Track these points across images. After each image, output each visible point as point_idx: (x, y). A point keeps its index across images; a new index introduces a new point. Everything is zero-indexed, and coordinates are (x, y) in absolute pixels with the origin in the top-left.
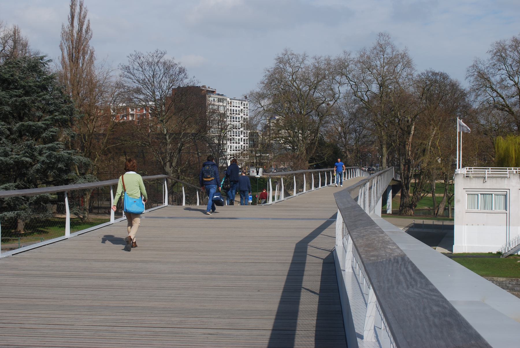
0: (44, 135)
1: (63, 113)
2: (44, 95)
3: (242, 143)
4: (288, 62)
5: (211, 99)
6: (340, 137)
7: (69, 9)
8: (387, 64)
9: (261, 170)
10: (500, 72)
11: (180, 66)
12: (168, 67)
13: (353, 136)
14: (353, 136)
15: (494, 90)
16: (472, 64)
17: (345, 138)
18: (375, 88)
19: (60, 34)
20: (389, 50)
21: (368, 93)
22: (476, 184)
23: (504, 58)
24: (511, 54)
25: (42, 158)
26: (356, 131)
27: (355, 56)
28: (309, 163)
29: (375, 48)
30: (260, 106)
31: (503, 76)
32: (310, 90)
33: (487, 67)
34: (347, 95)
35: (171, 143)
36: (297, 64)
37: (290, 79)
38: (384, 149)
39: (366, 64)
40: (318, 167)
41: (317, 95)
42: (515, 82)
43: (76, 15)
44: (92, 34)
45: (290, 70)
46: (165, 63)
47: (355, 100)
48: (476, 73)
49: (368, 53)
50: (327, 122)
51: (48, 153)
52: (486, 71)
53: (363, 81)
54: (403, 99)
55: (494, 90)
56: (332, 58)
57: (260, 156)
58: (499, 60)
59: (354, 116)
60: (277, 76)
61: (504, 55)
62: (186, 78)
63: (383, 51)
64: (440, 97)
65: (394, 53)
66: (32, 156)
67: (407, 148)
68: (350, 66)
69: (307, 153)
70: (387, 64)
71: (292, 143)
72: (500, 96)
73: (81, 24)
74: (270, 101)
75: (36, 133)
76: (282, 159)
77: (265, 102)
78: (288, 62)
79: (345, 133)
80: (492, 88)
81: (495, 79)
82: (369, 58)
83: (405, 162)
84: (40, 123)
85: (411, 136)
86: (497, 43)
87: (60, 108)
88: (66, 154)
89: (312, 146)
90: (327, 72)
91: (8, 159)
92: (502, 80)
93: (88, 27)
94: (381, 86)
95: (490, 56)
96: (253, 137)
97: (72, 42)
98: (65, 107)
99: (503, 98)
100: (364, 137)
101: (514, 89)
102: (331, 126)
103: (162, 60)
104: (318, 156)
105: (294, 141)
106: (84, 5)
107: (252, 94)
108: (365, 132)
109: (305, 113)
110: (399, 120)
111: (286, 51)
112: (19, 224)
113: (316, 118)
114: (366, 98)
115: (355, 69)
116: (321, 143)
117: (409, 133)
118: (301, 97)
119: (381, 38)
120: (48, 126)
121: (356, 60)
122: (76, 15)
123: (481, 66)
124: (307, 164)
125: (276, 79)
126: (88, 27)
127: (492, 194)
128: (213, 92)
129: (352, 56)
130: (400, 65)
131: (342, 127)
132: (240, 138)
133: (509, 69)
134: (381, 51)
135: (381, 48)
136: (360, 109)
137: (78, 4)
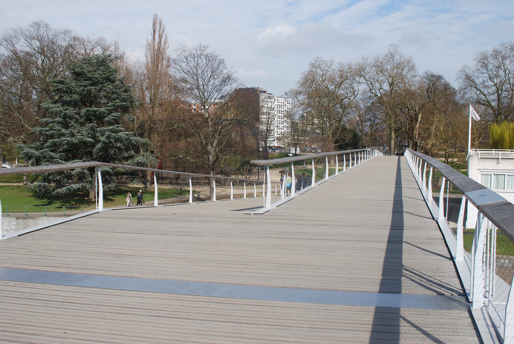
0: (106, 119)
1: (123, 100)
2: (108, 85)
3: (285, 129)
4: (319, 66)
5: (262, 96)
6: (358, 125)
7: (152, 26)
8: (396, 68)
9: (298, 149)
10: (483, 75)
11: (219, 57)
12: (209, 58)
13: (368, 124)
14: (368, 124)
15: (477, 89)
16: (461, 69)
17: (362, 125)
18: (386, 87)
19: (145, 45)
20: (397, 57)
21: (381, 91)
22: (490, 165)
23: (486, 65)
24: (492, 61)
25: (102, 139)
26: (370, 120)
27: (371, 61)
28: (335, 144)
29: (387, 56)
30: (297, 100)
31: (485, 79)
32: (336, 88)
33: (472, 72)
34: (365, 92)
35: (212, 126)
36: (326, 68)
37: (321, 79)
38: (393, 134)
39: (380, 68)
40: (341, 148)
41: (341, 92)
42: (494, 83)
43: (157, 28)
44: (169, 45)
45: (320, 72)
46: (207, 56)
47: (370, 96)
48: (464, 76)
49: (381, 59)
50: (348, 113)
51: (107, 133)
52: (472, 74)
53: (377, 80)
54: (409, 94)
55: (477, 89)
56: (353, 64)
57: (298, 139)
58: (482, 66)
59: (369, 109)
60: (310, 77)
61: (486, 62)
62: (226, 68)
63: (393, 58)
64: (437, 95)
65: (402, 59)
66: (94, 137)
67: (415, 133)
68: (367, 69)
69: (333, 136)
70: (396, 68)
71: (322, 129)
72: (483, 94)
73: (160, 37)
74: (305, 97)
75: (100, 119)
76: (314, 140)
77: (301, 97)
78: (319, 66)
79: (362, 122)
80: (476, 87)
81: (478, 81)
82: (382, 63)
83: (413, 144)
84: (103, 109)
85: (418, 122)
86: (481, 53)
87: (121, 96)
88: (123, 135)
89: (337, 131)
90: (349, 75)
91: (73, 139)
92: (484, 82)
93: (166, 39)
94: (391, 85)
95: (475, 63)
96: (294, 125)
97: (154, 50)
98: (124, 95)
99: (485, 96)
100: (377, 125)
101: (494, 89)
102: (351, 116)
103: (205, 53)
104: (342, 139)
105: (323, 127)
106: (163, 23)
107: (291, 91)
108: (377, 121)
109: (332, 106)
110: (409, 109)
111: (318, 58)
112: (90, 193)
113: (340, 110)
114: (379, 95)
115: (371, 72)
116: (344, 129)
117: (417, 120)
118: (328, 94)
119: (392, 48)
120: (110, 112)
121: (372, 64)
122: (157, 28)
123: (468, 72)
124: (333, 145)
125: (310, 79)
126: (166, 39)
127: (505, 175)
128: (265, 92)
129: (369, 61)
130: (406, 69)
131: (360, 117)
132: (284, 125)
133: (490, 73)
134: (391, 58)
135: (392, 56)
136: (373, 103)
137: (159, 22)
